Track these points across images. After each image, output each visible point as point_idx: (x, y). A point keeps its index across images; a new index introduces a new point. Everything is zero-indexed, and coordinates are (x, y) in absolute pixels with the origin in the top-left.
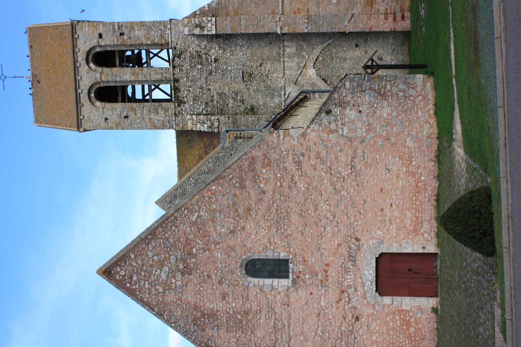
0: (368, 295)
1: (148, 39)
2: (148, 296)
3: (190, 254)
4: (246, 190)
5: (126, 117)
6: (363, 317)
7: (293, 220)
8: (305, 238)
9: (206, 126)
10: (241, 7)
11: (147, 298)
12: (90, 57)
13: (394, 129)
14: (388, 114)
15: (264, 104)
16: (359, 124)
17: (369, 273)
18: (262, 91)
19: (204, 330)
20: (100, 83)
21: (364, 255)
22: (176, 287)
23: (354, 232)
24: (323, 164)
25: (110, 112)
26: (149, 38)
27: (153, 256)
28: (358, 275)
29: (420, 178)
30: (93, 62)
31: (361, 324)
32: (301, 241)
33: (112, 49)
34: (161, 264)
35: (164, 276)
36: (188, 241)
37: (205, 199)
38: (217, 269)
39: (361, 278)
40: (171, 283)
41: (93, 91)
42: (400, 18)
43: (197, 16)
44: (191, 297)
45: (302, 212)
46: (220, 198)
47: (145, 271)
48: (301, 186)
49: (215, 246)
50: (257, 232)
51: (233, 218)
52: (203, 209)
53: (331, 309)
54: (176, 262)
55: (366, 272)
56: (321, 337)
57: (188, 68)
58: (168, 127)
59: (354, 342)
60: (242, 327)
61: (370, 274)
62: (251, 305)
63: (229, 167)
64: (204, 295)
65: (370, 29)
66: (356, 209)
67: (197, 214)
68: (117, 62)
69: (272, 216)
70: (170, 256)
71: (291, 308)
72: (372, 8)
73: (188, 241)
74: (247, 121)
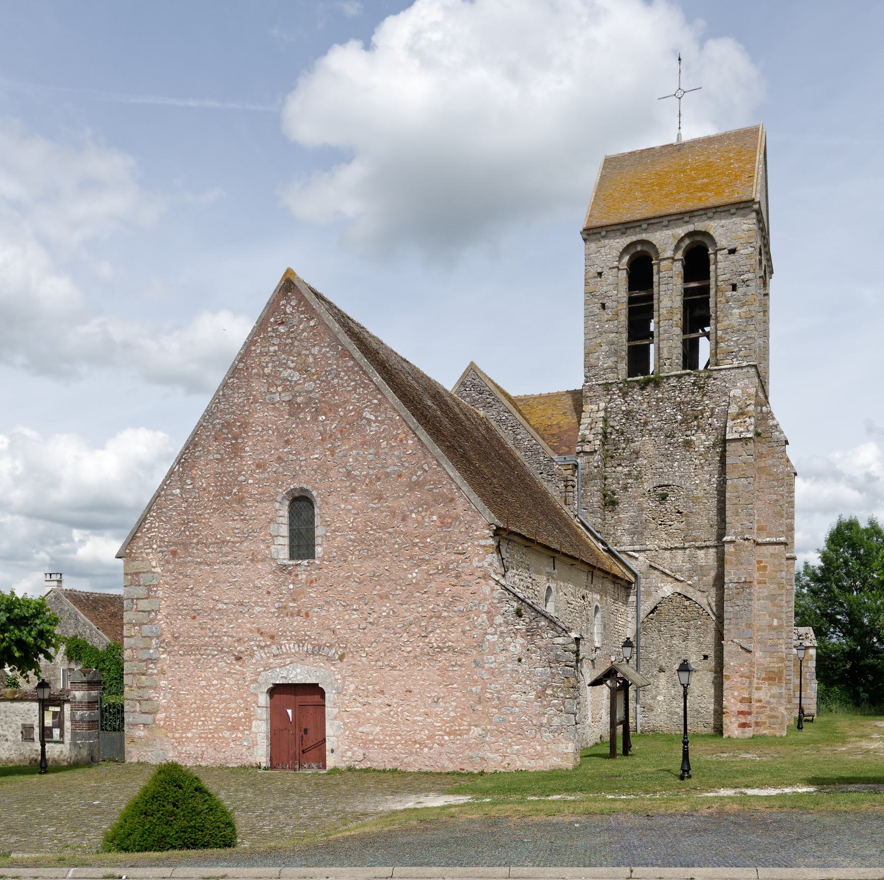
0: (269, 673)
1: (725, 330)
2: (258, 351)
3: (318, 412)
4: (407, 492)
5: (603, 306)
6: (240, 666)
7: (366, 564)
8: (343, 582)
9: (587, 432)
10: (772, 478)
11: (255, 350)
12: (698, 238)
13: (494, 710)
14: (515, 701)
15: (620, 521)
16: (501, 658)
17: (298, 675)
18: (640, 515)
19: (216, 440)
20: (657, 259)
21: (321, 667)
22: (271, 393)
23: (352, 653)
24: (445, 606)
25: (611, 279)
26: (727, 333)
27: (313, 355)
28: (294, 659)
29: (426, 746)
30: (692, 243)
31: (231, 663)
32: (339, 576)
33: (712, 274)
34: (303, 369)
35: (285, 374)
36: (334, 408)
37: (394, 429)
38: (298, 453)
39: (291, 663)
40: (277, 386)
41: (645, 248)
42: (743, 721)
43: (759, 408)
44: (258, 417)
45: (378, 576)
46: (396, 453)
47: (292, 344)
48: (414, 575)
49: (329, 449)
50: (349, 510)
51: (368, 474)
52: (380, 428)
53: (249, 622)
54: (306, 391)
55: (298, 670)
56: (213, 608)
57: (678, 399)
58: (588, 375)
59: (209, 655)
60: (222, 495)
61: (296, 676)
62: (251, 506)
63: (439, 465)
64: (262, 437)
65: (728, 677)
66: (382, 654)
67: (373, 418)
68: (693, 285)
69: (371, 532)
70: (314, 381)
71: (248, 565)
72: (764, 679)
73: (334, 408)
74: (592, 495)
